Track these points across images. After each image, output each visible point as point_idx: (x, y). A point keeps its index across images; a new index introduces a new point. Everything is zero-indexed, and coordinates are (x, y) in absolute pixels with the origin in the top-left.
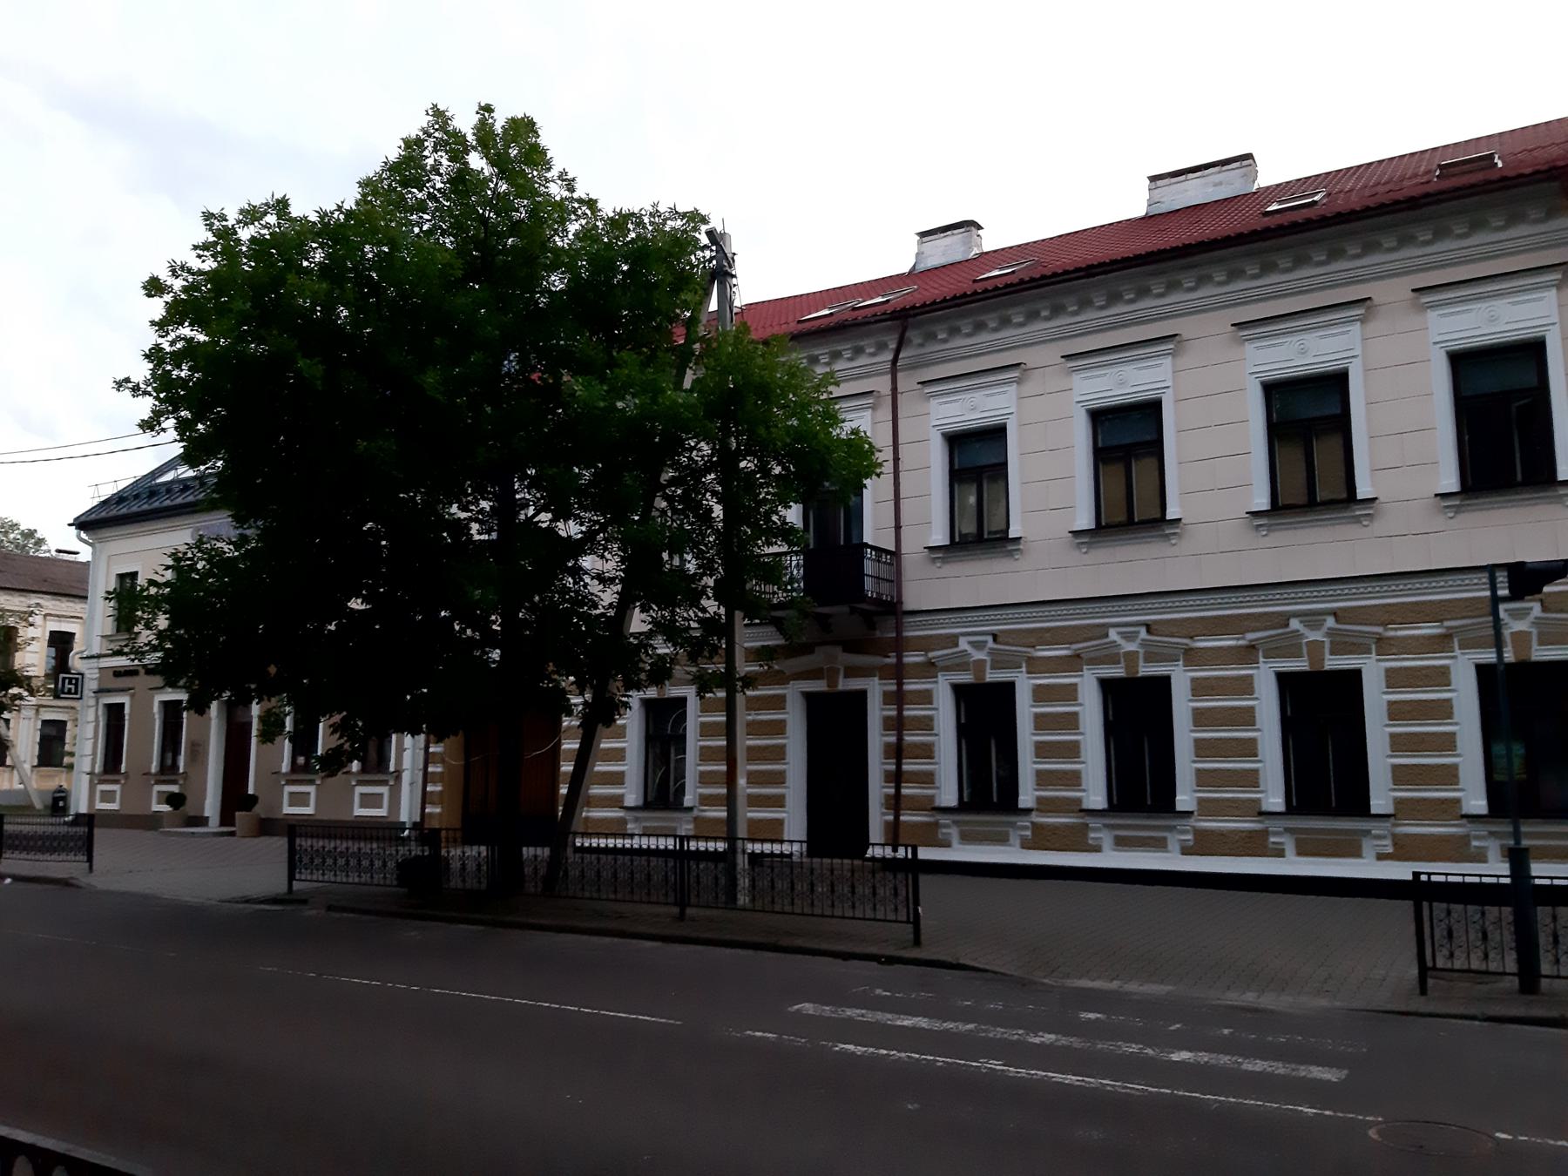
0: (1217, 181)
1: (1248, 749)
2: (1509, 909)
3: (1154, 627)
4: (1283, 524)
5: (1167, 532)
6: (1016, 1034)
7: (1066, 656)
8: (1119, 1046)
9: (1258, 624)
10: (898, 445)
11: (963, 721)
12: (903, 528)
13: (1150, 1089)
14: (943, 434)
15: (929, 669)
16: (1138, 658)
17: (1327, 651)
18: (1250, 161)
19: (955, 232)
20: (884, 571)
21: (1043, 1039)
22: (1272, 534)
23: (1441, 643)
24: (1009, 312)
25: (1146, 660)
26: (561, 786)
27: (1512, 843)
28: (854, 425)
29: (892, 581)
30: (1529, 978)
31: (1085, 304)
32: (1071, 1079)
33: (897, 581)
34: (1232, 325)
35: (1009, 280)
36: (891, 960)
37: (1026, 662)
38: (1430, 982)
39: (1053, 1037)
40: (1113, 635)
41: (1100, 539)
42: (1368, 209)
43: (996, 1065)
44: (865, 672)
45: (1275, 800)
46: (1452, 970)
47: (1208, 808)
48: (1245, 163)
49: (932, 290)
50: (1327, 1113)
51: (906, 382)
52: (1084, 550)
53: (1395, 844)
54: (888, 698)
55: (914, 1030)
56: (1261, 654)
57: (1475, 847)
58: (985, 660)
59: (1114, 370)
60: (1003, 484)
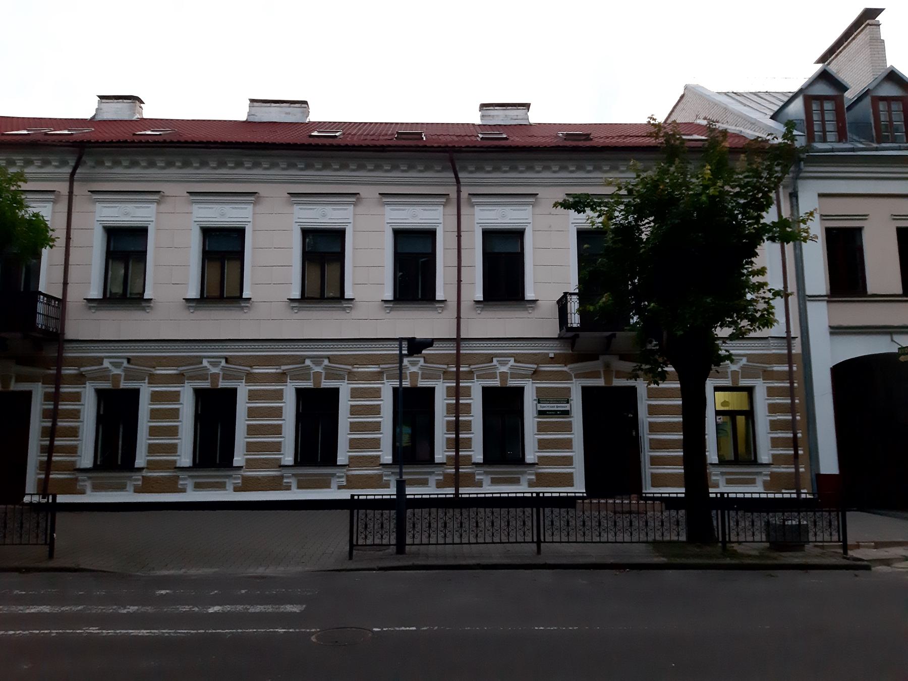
0: (287, 111)
1: (277, 430)
2: (395, 511)
3: (230, 359)
4: (307, 307)
5: (243, 305)
6: (111, 609)
7: (175, 374)
8: (178, 608)
9: (289, 361)
10: (70, 228)
11: (102, 413)
12: (70, 284)
13: (192, 631)
14: (301, 228)
15: (80, 379)
16: (219, 377)
17: (323, 377)
18: (306, 106)
19: (125, 101)
20: (53, 312)
21: (129, 610)
22: (196, 312)
23: (378, 376)
24: (244, 159)
25: (223, 379)
26: (799, 448)
27: (398, 477)
28: (36, 211)
29: (58, 319)
30: (401, 546)
31: (204, 164)
32: (144, 632)
33: (61, 319)
34: (288, 193)
35: (156, 139)
36: (28, 570)
37: (149, 376)
38: (355, 552)
39: (136, 608)
40: (205, 363)
41: (202, 305)
42: (361, 146)
43: (94, 630)
44: (32, 379)
45: (288, 458)
46: (366, 545)
47: (250, 464)
48: (303, 105)
49: (104, 134)
50: (291, 630)
51: (80, 189)
52: (192, 311)
53: (347, 481)
54: (47, 397)
55: (260, 614)
56: (288, 379)
57: (478, 479)
58: (738, 372)
59: (499, 208)
60: (338, 267)
